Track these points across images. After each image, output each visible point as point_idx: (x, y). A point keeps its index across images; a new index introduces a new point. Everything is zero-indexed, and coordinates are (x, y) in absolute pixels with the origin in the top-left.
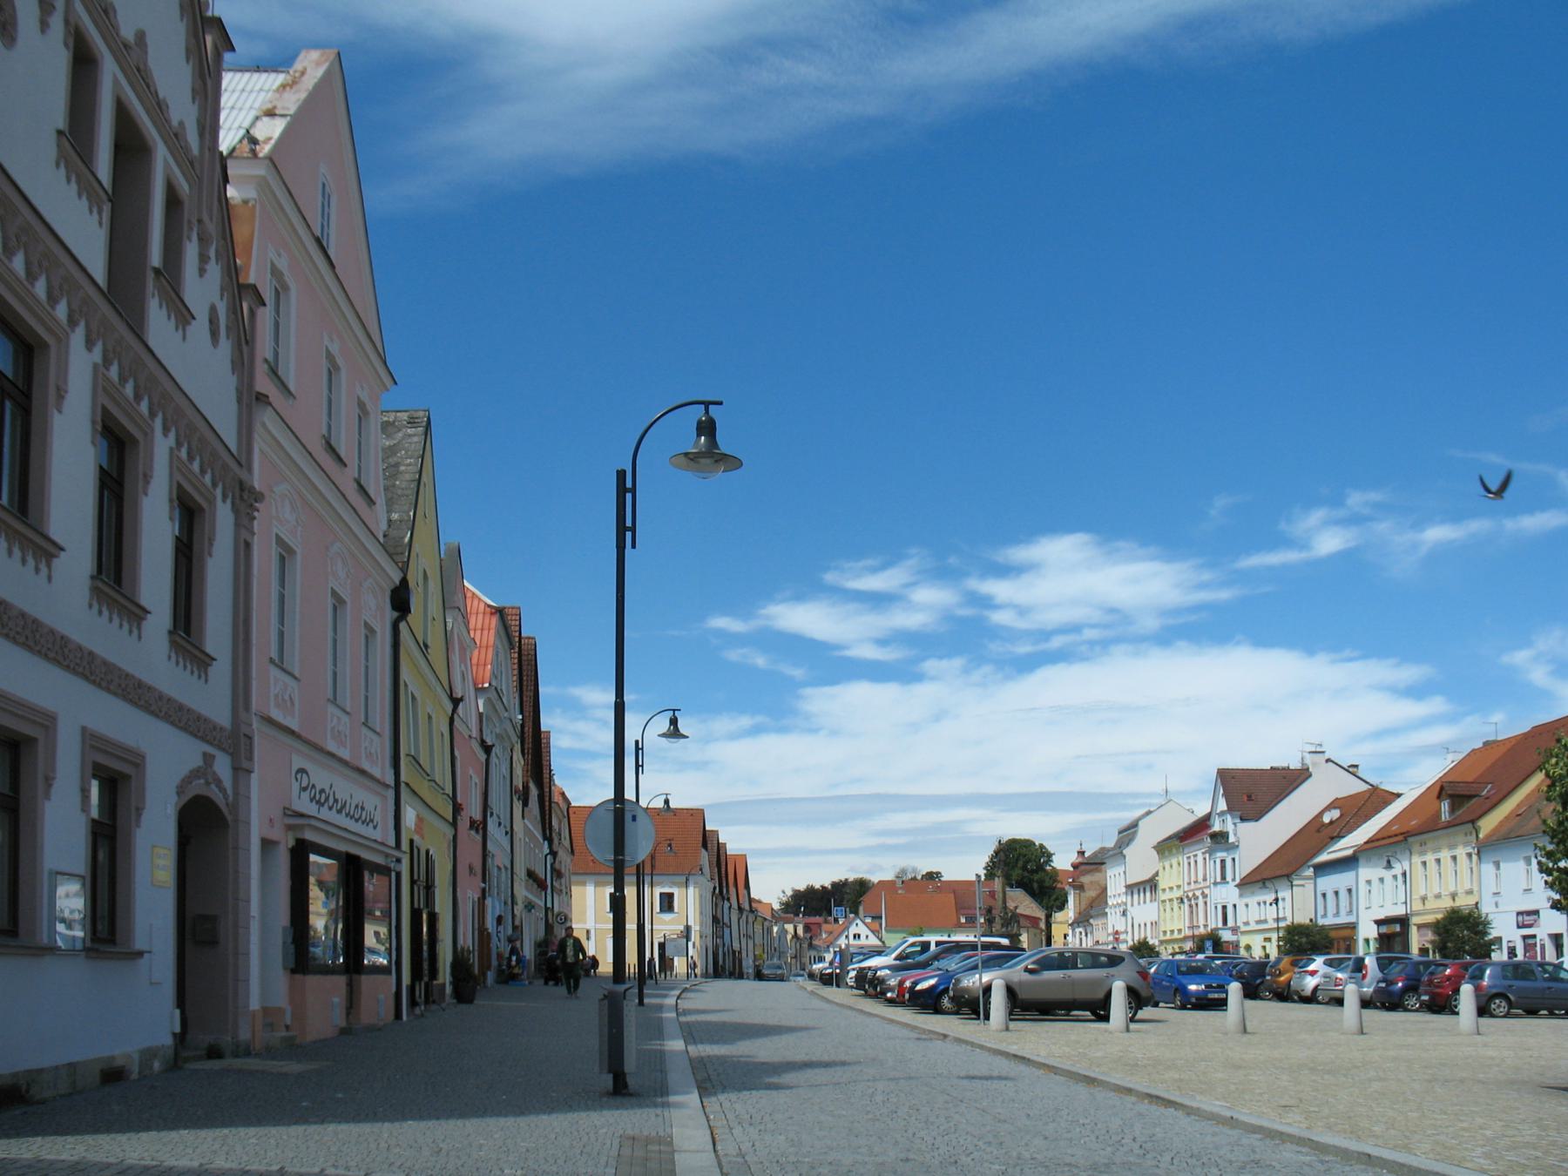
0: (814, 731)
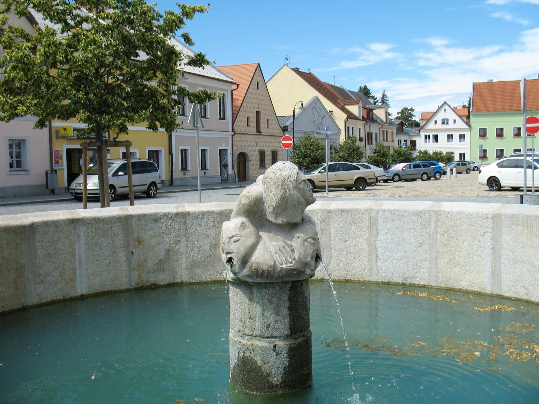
0: (523, 51)
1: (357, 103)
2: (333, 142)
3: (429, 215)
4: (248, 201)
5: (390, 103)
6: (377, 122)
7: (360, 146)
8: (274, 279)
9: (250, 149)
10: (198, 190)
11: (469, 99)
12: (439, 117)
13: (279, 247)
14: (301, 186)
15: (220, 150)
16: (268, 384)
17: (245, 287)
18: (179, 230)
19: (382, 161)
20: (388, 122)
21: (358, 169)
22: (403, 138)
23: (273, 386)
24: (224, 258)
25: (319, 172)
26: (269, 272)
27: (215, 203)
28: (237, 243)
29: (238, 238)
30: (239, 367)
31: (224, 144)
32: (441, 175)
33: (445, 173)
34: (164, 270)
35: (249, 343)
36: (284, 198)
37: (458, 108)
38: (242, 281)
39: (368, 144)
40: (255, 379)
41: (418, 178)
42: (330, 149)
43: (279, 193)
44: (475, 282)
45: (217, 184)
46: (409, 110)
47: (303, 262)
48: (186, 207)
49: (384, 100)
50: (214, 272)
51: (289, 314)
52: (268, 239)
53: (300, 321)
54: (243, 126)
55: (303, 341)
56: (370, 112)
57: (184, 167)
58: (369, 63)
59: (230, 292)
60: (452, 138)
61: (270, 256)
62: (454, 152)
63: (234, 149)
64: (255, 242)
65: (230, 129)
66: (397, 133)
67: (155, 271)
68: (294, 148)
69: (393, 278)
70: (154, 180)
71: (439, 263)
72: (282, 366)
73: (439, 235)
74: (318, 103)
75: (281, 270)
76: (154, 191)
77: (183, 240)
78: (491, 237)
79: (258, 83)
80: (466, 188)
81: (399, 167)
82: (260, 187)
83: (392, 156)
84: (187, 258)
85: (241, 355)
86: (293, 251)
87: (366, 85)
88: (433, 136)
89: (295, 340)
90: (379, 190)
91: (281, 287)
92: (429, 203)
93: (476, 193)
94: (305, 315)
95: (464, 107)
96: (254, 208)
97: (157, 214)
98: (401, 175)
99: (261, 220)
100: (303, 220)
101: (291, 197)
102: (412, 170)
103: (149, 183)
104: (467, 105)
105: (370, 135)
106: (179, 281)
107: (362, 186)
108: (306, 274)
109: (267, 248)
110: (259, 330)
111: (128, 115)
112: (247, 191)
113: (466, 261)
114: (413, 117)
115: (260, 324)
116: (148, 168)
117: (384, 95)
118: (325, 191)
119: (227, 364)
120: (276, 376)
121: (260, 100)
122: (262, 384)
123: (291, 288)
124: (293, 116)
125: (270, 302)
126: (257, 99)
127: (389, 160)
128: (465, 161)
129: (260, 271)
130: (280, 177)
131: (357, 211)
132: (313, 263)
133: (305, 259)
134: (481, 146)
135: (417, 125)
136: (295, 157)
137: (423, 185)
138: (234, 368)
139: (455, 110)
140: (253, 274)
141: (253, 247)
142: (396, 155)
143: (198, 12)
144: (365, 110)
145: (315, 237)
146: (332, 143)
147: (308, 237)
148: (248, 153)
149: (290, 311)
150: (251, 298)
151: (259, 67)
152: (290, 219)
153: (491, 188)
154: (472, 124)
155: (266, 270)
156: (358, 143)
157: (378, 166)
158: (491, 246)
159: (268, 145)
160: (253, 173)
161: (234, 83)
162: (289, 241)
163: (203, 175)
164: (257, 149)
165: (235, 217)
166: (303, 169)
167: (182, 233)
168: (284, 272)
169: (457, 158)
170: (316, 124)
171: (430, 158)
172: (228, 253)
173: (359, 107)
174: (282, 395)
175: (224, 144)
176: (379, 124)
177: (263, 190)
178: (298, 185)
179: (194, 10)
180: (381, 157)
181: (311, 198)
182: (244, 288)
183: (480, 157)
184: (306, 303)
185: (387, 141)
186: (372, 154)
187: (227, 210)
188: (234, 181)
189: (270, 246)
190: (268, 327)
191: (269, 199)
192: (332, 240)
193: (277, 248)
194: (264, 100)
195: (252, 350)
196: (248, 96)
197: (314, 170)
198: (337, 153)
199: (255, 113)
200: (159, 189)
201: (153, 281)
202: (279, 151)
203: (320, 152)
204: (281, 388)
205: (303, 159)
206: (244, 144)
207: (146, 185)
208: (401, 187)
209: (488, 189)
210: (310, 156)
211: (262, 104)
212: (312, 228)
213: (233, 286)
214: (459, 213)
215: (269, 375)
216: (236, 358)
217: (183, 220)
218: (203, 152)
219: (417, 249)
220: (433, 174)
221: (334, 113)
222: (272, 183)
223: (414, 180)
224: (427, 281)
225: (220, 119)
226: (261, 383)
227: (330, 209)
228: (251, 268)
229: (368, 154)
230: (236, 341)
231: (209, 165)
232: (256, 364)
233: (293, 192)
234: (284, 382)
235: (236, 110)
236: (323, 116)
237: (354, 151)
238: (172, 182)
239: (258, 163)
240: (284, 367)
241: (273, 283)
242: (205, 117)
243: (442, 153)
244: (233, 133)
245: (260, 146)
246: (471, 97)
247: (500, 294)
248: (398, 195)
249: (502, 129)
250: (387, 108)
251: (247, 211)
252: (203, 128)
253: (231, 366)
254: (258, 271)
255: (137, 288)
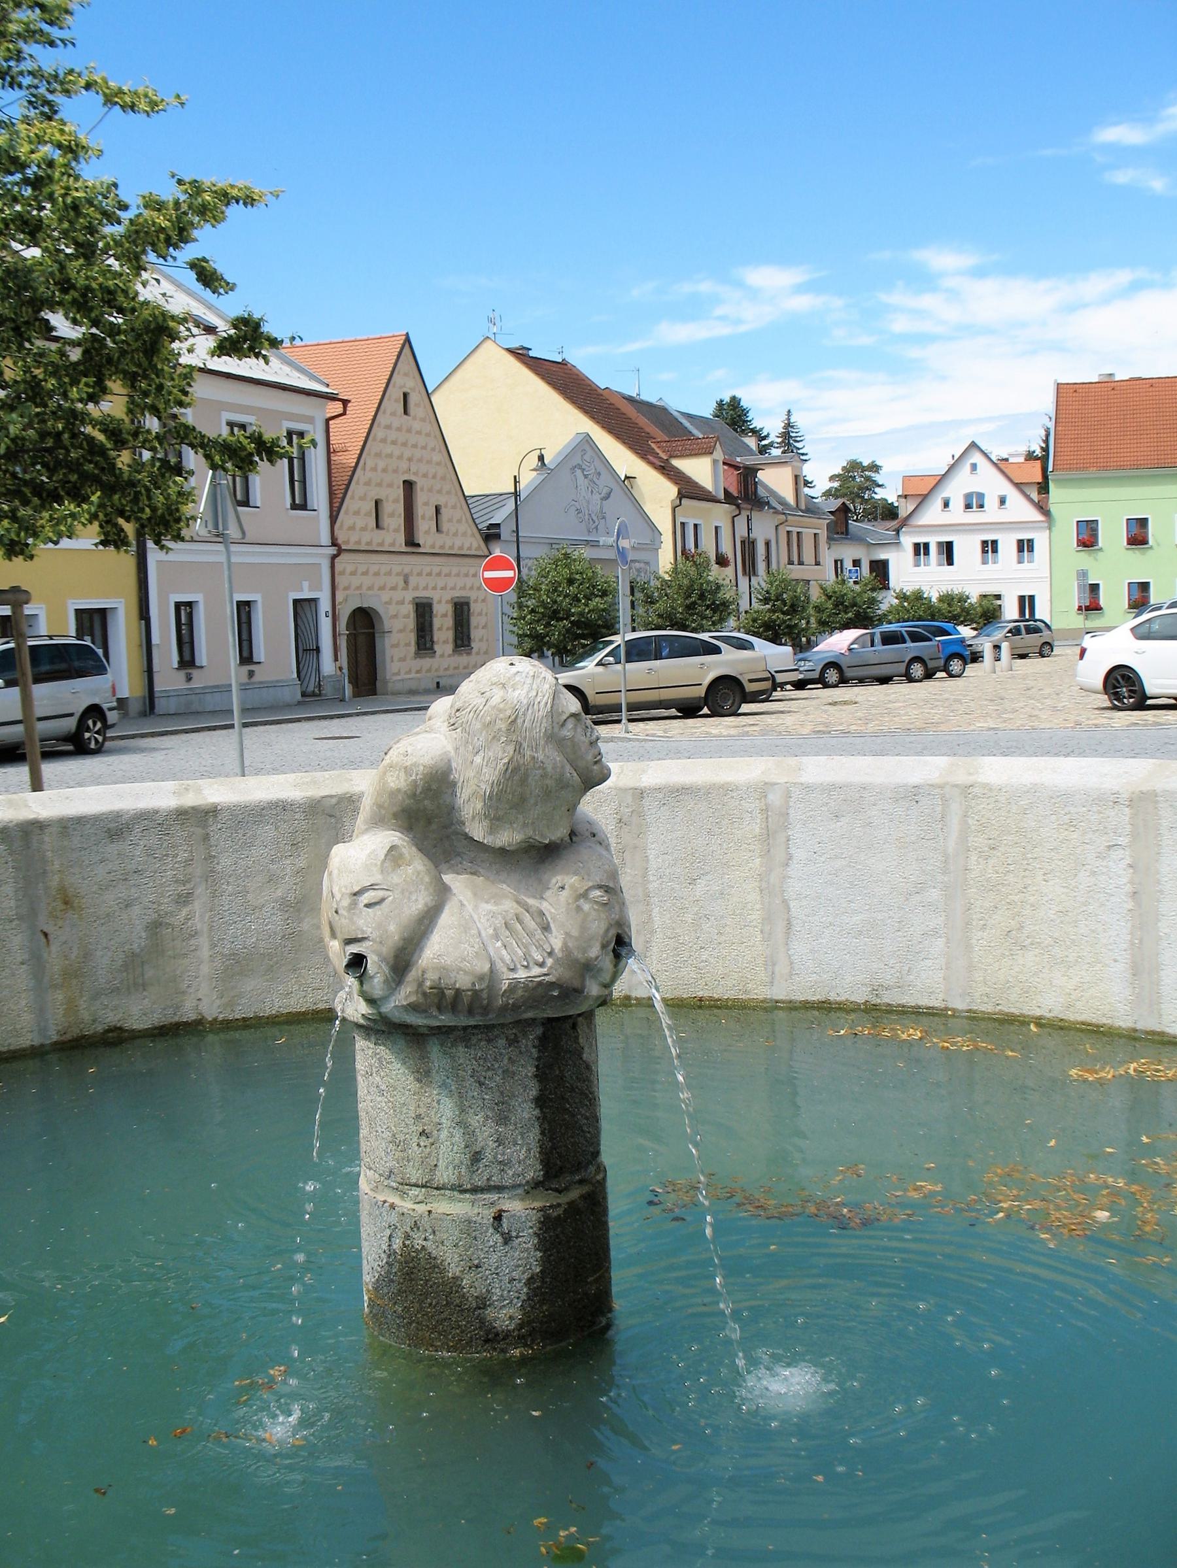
1: (705, 451)
2: (638, 570)
3: (943, 797)
4: (406, 780)
5: (807, 447)
6: (771, 507)
7: (721, 582)
8: (491, 1016)
9: (385, 596)
10: (232, 726)
11: (1043, 433)
12: (956, 490)
13: (504, 918)
14: (567, 732)
15: (296, 602)
16: (480, 1328)
17: (403, 1042)
18: (188, 862)
19: (789, 627)
20: (803, 507)
21: (716, 650)
22: (848, 553)
23: (497, 1334)
24: (340, 956)
25: (597, 665)
26: (476, 994)
27: (293, 776)
28: (376, 912)
29: (381, 894)
30: (392, 1281)
31: (306, 584)
32: (965, 663)
33: (976, 657)
34: (144, 986)
35: (422, 1209)
36: (516, 770)
37: (1011, 460)
38: (395, 1024)
39: (744, 573)
40: (443, 1316)
41: (896, 673)
42: (628, 592)
43: (501, 754)
44: (1082, 996)
45: (288, 706)
46: (864, 469)
47: (577, 960)
48: (206, 792)
49: (788, 438)
50: (296, 987)
51: (538, 1118)
52: (469, 894)
53: (573, 1137)
54: (364, 529)
55: (583, 1197)
56: (748, 475)
57: (187, 657)
58: (742, 329)
59: (358, 1057)
60: (995, 551)
61: (477, 946)
62: (1002, 593)
63: (339, 598)
64: (431, 904)
65: (325, 539)
66: (830, 539)
67: (118, 988)
68: (521, 591)
69: (839, 990)
70: (96, 701)
71: (974, 941)
72: (523, 1273)
73: (974, 858)
74: (590, 453)
75: (513, 988)
76: (96, 733)
77: (199, 891)
78: (1128, 861)
79: (405, 395)
80: (1042, 704)
81: (840, 642)
82: (442, 738)
83: (819, 609)
84: (213, 946)
85: (397, 1244)
86: (546, 928)
87: (738, 395)
88: (940, 544)
89: (557, 1194)
90: (782, 712)
91: (512, 1037)
92: (942, 761)
93: (1072, 718)
94: (587, 1118)
95: (1030, 456)
96: (426, 802)
97: (118, 815)
98: (844, 668)
99: (448, 837)
100: (573, 834)
101: (537, 765)
102: (879, 652)
103: (81, 709)
104: (1038, 452)
105: (748, 546)
106: (192, 1016)
107: (730, 702)
108: (586, 998)
109: (466, 926)
110: (451, 1167)
111: (19, 514)
112: (402, 750)
113: (1056, 935)
114: (877, 490)
115: (452, 1150)
116: (76, 664)
117: (789, 425)
118: (619, 721)
119: (356, 1270)
120: (504, 1306)
121: (415, 446)
122: (462, 1332)
123: (543, 1041)
124: (516, 494)
125: (481, 1084)
126: (404, 444)
127: (808, 623)
128: (1036, 621)
129: (448, 993)
130: (501, 706)
131: (726, 789)
132: (607, 962)
133: (585, 951)
134: (1083, 574)
135: (890, 512)
136: (524, 618)
137: (913, 697)
138: (377, 1288)
139: (1002, 465)
140: (429, 1000)
141: (426, 922)
142: (829, 605)
143: (237, 202)
144: (732, 470)
145: (611, 885)
146: (633, 574)
147: (591, 884)
148: (381, 610)
149: (541, 1110)
150: (423, 1075)
151: (407, 349)
152: (534, 831)
153: (1116, 703)
154: (1053, 509)
155: (468, 990)
156: (715, 573)
157: (775, 640)
158: (1129, 888)
159: (441, 584)
160: (396, 671)
161: (332, 398)
162: (534, 897)
163: (245, 679)
164: (409, 596)
165: (367, 830)
166: (550, 653)
167: (198, 869)
168: (520, 993)
169: (1010, 611)
170: (587, 517)
171: (932, 613)
172: (349, 942)
173: (715, 462)
174: (523, 1361)
175: (306, 584)
176: (777, 512)
177: (450, 748)
178: (556, 730)
179: (225, 197)
180: (784, 613)
181: (595, 767)
182: (401, 1043)
183: (1080, 608)
184: (589, 1081)
185: (801, 563)
186: (756, 605)
187: (331, 796)
188: (340, 696)
189: (476, 917)
190: (476, 1157)
191: (471, 773)
192: (651, 878)
193: (499, 922)
194: (424, 448)
195: (430, 1230)
196: (375, 435)
197: (582, 658)
198: (651, 603)
199: (399, 487)
200: (113, 726)
201: (111, 1018)
202: (476, 601)
203: (596, 602)
204: (521, 1340)
205: (548, 625)
206: (367, 581)
207: (71, 715)
208: (845, 703)
209: (1108, 704)
210: (568, 615)
211: (420, 460)
212: (600, 856)
213: (367, 1037)
214: (1033, 790)
215: (483, 1303)
216: (383, 1255)
217: (199, 831)
218: (244, 609)
219: (907, 899)
220: (942, 662)
221: (639, 481)
222: (478, 726)
223: (884, 680)
224: (941, 997)
225: (294, 507)
226: (460, 1326)
227: (643, 785)
228: (420, 984)
229: (744, 605)
230: (380, 1204)
231: (262, 648)
232: (443, 1271)
233: (544, 750)
234: (529, 1323)
235: (341, 478)
236: (605, 490)
237: (702, 596)
238: (150, 704)
239: (412, 637)
240: (526, 1276)
241: (489, 1028)
242: (246, 503)
243: (968, 598)
244: (333, 551)
245: (416, 588)
246: (1051, 425)
247: (1157, 1028)
248: (841, 728)
249: (1143, 522)
250: (799, 464)
251: (403, 811)
252: (243, 538)
253: (368, 1278)
254: (443, 993)
255: (63, 1043)
